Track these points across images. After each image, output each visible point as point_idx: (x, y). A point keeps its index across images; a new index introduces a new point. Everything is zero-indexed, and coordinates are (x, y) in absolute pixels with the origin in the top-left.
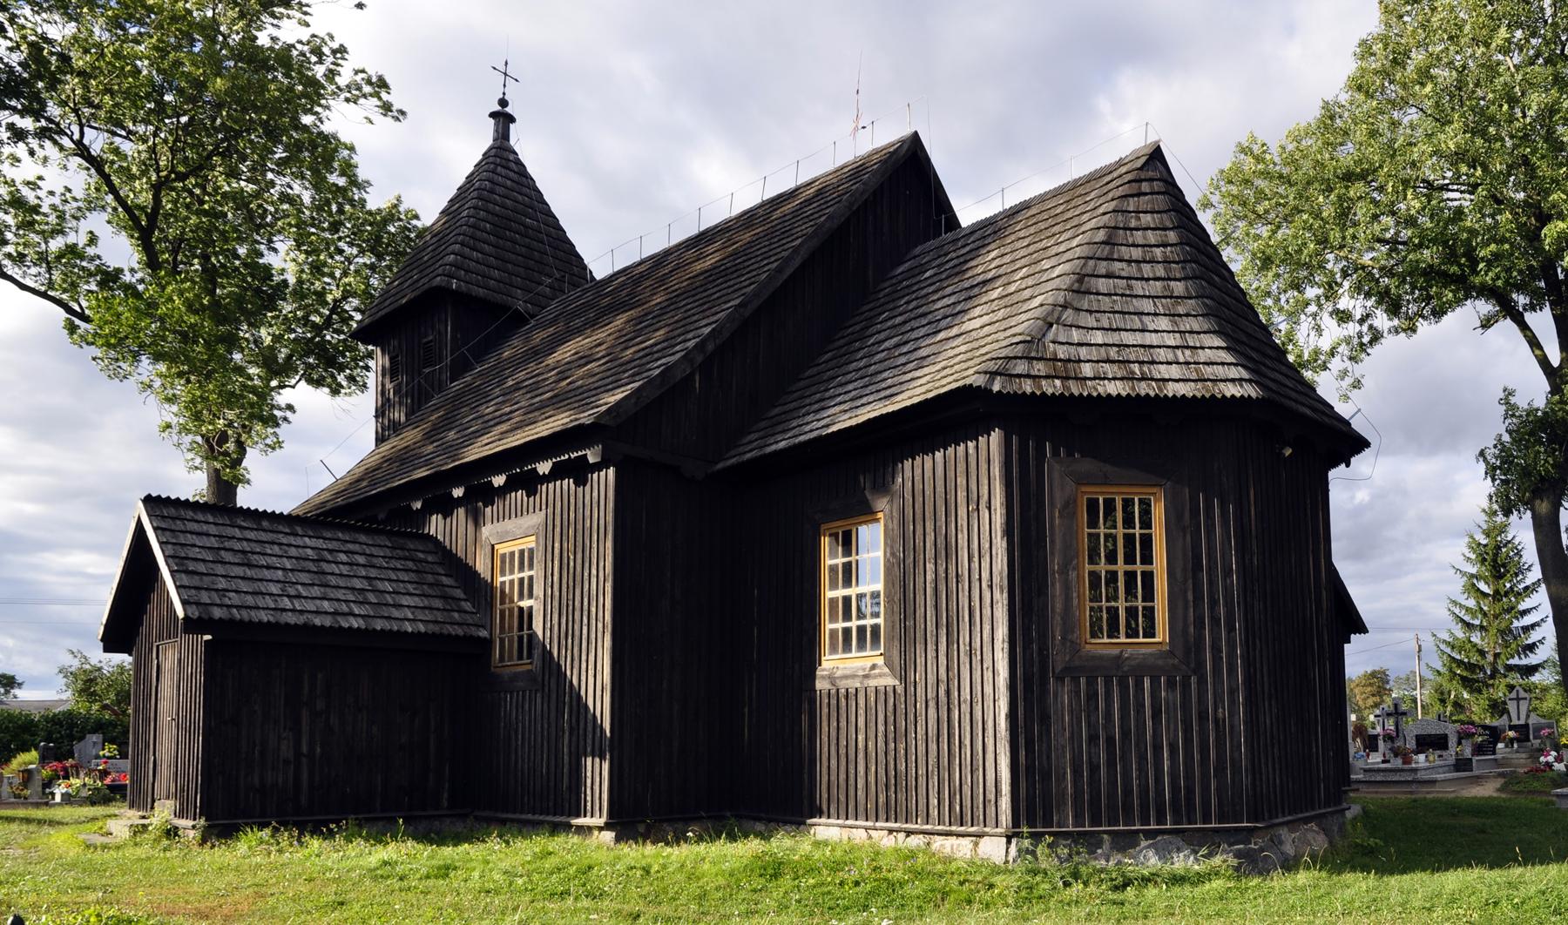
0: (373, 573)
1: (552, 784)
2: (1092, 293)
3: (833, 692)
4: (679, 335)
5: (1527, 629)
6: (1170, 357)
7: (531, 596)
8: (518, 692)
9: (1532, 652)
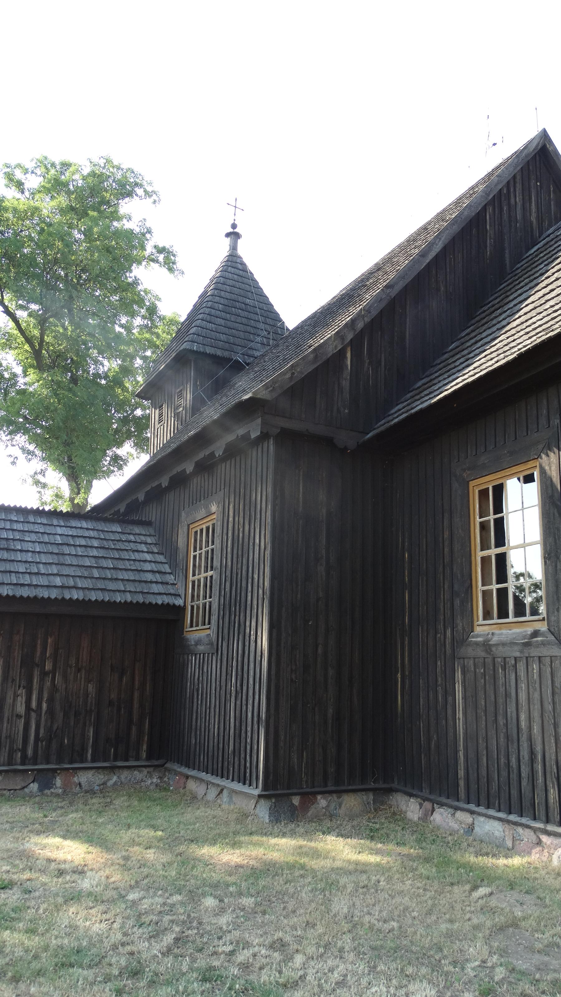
1: (221, 746)
3: (489, 661)
8: (200, 654)
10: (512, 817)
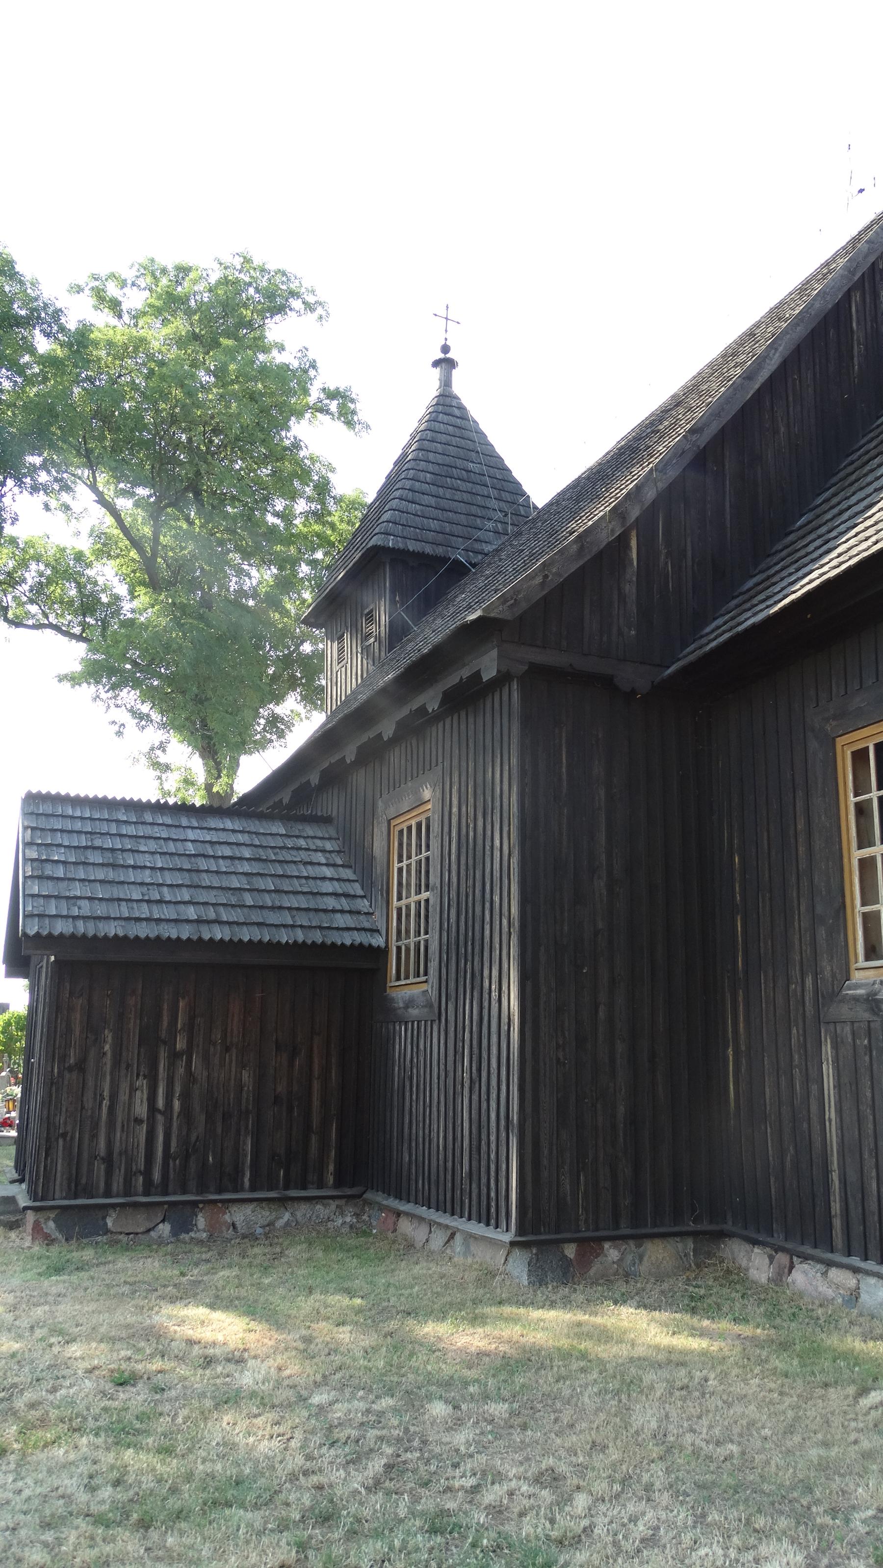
7: (427, 888)
8: (413, 1022)
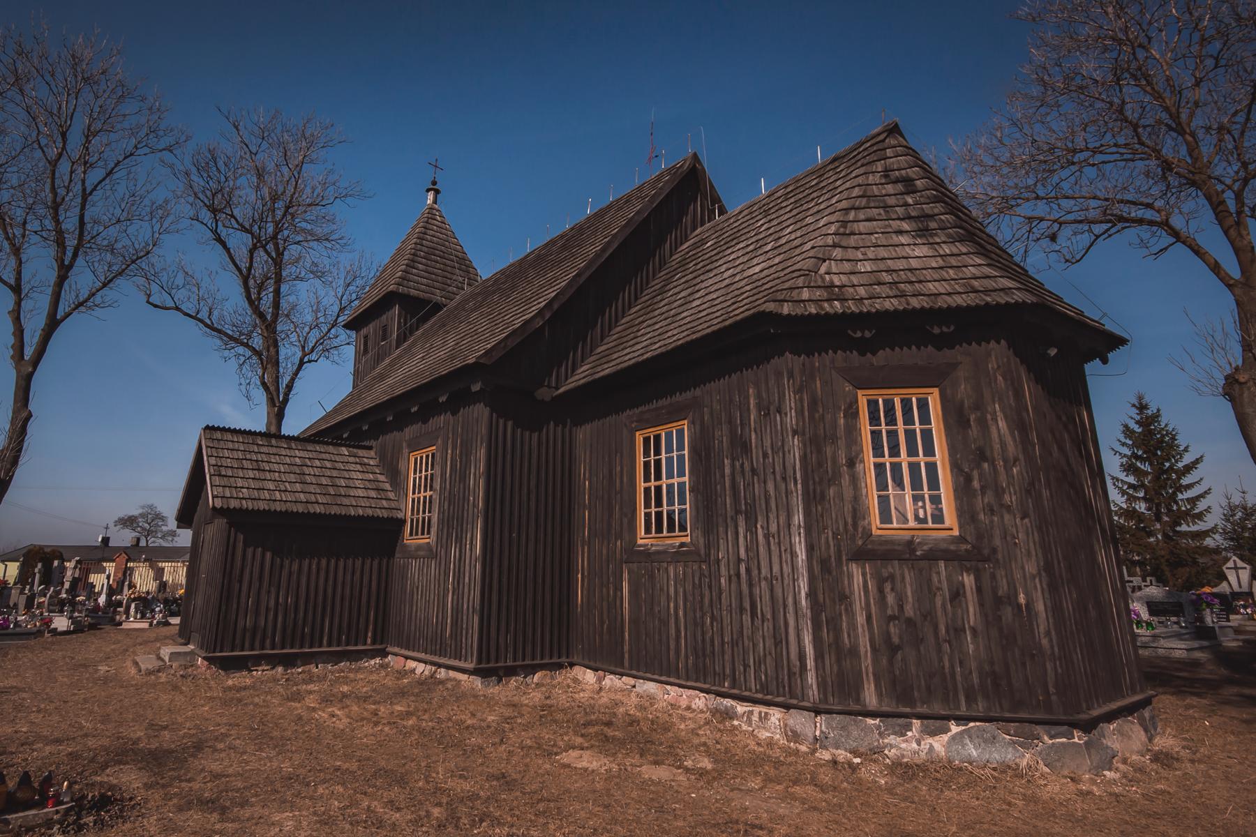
0: (335, 473)
1: (439, 632)
2: (856, 234)
4: (534, 301)
5: (1193, 501)
6: (936, 276)
9: (1201, 520)
10: (663, 678)
